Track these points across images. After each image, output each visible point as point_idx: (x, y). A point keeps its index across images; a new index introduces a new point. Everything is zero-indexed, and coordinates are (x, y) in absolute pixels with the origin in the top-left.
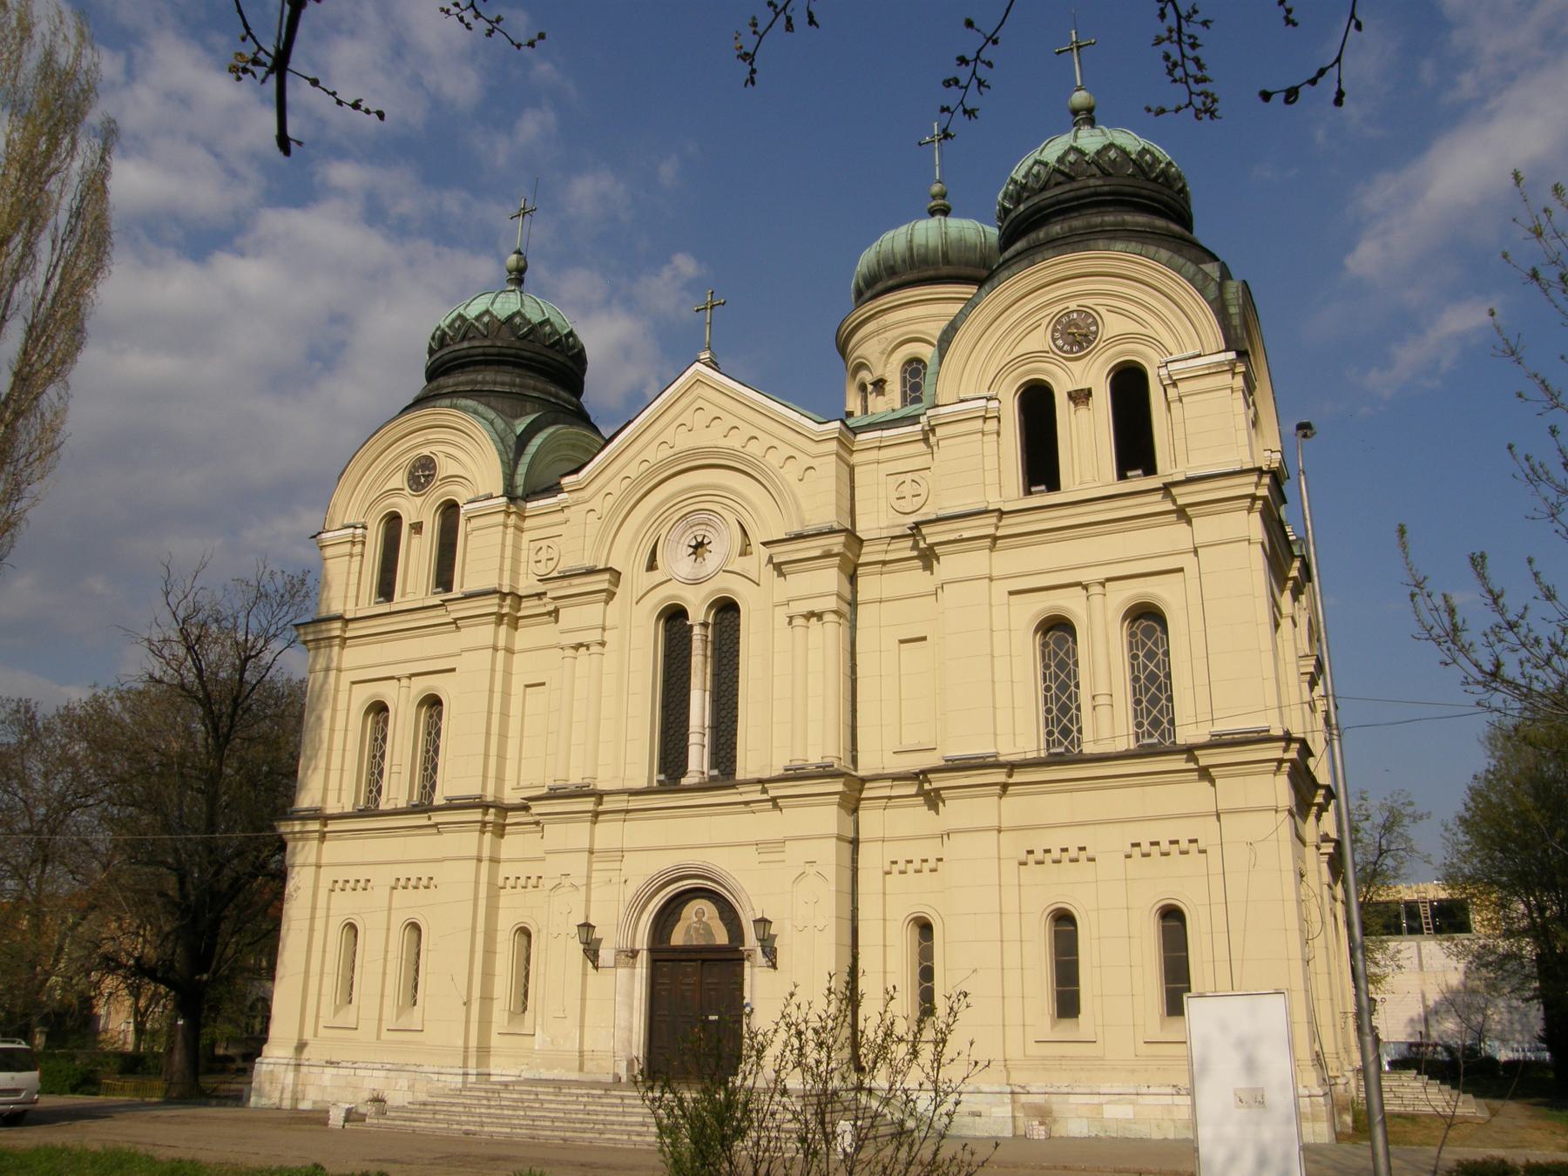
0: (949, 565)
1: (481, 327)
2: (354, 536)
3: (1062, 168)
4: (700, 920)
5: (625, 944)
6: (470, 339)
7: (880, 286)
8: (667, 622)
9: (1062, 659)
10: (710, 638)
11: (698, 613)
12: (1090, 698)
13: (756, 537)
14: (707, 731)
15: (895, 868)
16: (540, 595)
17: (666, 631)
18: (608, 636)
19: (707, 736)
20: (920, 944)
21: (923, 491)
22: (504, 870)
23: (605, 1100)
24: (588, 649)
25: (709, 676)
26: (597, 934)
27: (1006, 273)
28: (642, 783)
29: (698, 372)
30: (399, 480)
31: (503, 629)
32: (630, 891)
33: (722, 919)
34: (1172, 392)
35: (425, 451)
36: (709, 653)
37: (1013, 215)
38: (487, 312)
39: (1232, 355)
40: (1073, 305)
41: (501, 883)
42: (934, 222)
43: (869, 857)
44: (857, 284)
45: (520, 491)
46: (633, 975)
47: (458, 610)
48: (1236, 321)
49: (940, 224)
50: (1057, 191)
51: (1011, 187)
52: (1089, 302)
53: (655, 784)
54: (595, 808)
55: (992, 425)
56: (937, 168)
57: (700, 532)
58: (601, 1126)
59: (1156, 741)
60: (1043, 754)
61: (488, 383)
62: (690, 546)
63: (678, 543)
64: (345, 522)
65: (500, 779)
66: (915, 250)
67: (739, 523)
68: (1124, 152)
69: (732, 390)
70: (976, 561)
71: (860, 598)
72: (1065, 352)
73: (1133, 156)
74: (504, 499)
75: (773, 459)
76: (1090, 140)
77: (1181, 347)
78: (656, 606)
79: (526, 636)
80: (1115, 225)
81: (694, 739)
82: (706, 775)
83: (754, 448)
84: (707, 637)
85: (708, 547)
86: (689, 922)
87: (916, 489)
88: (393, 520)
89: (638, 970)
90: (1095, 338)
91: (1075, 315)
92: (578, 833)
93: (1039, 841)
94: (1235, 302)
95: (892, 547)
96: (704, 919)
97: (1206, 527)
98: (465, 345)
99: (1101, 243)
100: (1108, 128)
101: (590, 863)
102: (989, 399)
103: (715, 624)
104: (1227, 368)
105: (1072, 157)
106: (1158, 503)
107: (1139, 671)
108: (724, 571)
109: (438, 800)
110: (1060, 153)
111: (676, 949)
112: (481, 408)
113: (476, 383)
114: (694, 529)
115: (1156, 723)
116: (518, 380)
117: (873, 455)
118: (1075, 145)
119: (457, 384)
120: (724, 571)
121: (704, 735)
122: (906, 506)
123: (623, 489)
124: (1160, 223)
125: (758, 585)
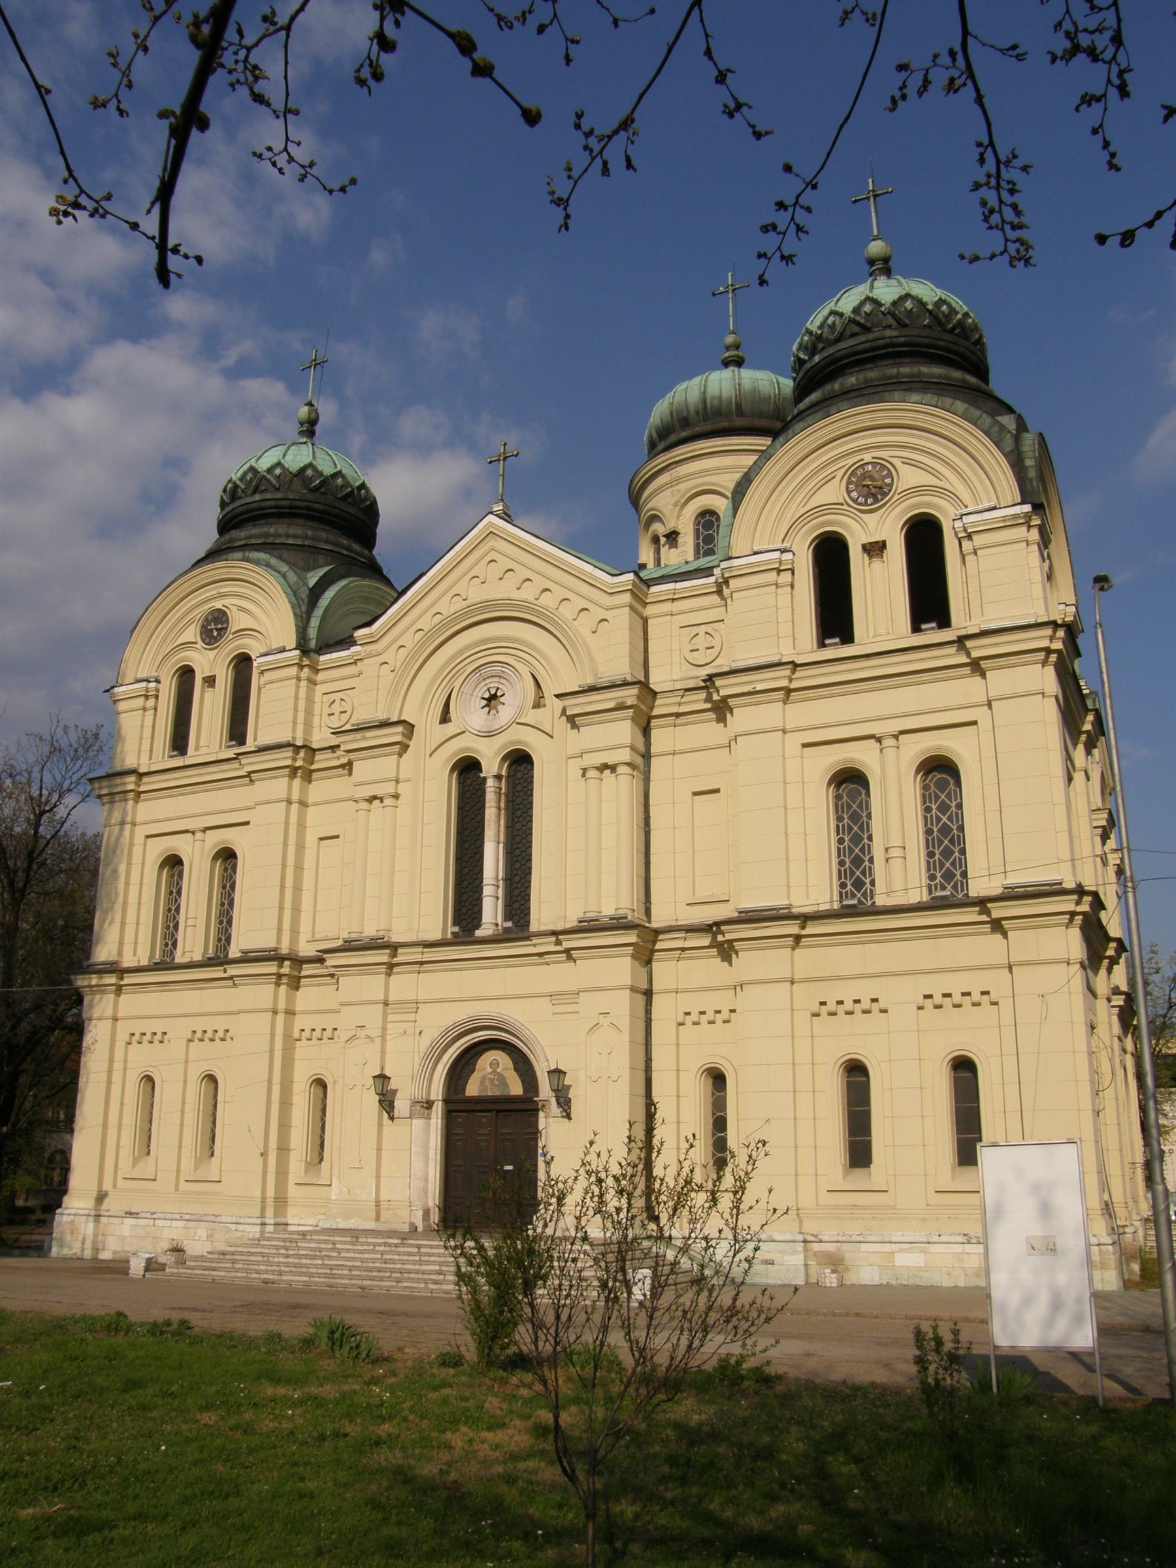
0: (742, 717)
1: (272, 480)
2: (147, 690)
3: (858, 318)
4: (494, 1072)
5: (421, 1095)
6: (262, 492)
10: (503, 791)
11: (491, 766)
13: (550, 690)
14: (501, 883)
16: (333, 748)
18: (401, 789)
20: (713, 1094)
21: (716, 643)
22: (300, 1022)
25: (502, 829)
26: (393, 1085)
27: (801, 425)
28: (436, 935)
30: (192, 633)
31: (297, 782)
32: (425, 1042)
33: (516, 1070)
34: (966, 545)
35: (218, 605)
36: (502, 805)
37: (808, 366)
38: (279, 464)
39: (1027, 508)
40: (868, 457)
41: (296, 1035)
46: (428, 1126)
47: (252, 763)
48: (1032, 474)
53: (449, 936)
55: (786, 577)
57: (493, 684)
60: (836, 906)
61: (280, 536)
62: (483, 698)
63: (472, 695)
64: (138, 676)
65: (295, 932)
68: (920, 302)
70: (771, 713)
71: (653, 750)
72: (860, 504)
73: (930, 307)
74: (297, 652)
75: (567, 612)
76: (886, 291)
77: (976, 498)
78: (447, 761)
79: (319, 790)
81: (487, 891)
82: (500, 927)
83: (547, 600)
84: (500, 789)
85: (502, 700)
86: (482, 1073)
88: (186, 674)
89: (433, 1121)
90: (890, 491)
91: (870, 467)
92: (372, 986)
94: (1031, 454)
96: (499, 1070)
97: (999, 680)
98: (257, 497)
99: (896, 395)
101: (385, 1015)
102: (783, 551)
103: (508, 776)
105: (868, 308)
107: (932, 824)
108: (518, 723)
109: (234, 952)
110: (856, 304)
112: (274, 561)
113: (269, 536)
114: (488, 681)
115: (948, 876)
117: (667, 607)
118: (871, 295)
120: (518, 723)
121: (498, 887)
124: (957, 374)
125: (552, 737)
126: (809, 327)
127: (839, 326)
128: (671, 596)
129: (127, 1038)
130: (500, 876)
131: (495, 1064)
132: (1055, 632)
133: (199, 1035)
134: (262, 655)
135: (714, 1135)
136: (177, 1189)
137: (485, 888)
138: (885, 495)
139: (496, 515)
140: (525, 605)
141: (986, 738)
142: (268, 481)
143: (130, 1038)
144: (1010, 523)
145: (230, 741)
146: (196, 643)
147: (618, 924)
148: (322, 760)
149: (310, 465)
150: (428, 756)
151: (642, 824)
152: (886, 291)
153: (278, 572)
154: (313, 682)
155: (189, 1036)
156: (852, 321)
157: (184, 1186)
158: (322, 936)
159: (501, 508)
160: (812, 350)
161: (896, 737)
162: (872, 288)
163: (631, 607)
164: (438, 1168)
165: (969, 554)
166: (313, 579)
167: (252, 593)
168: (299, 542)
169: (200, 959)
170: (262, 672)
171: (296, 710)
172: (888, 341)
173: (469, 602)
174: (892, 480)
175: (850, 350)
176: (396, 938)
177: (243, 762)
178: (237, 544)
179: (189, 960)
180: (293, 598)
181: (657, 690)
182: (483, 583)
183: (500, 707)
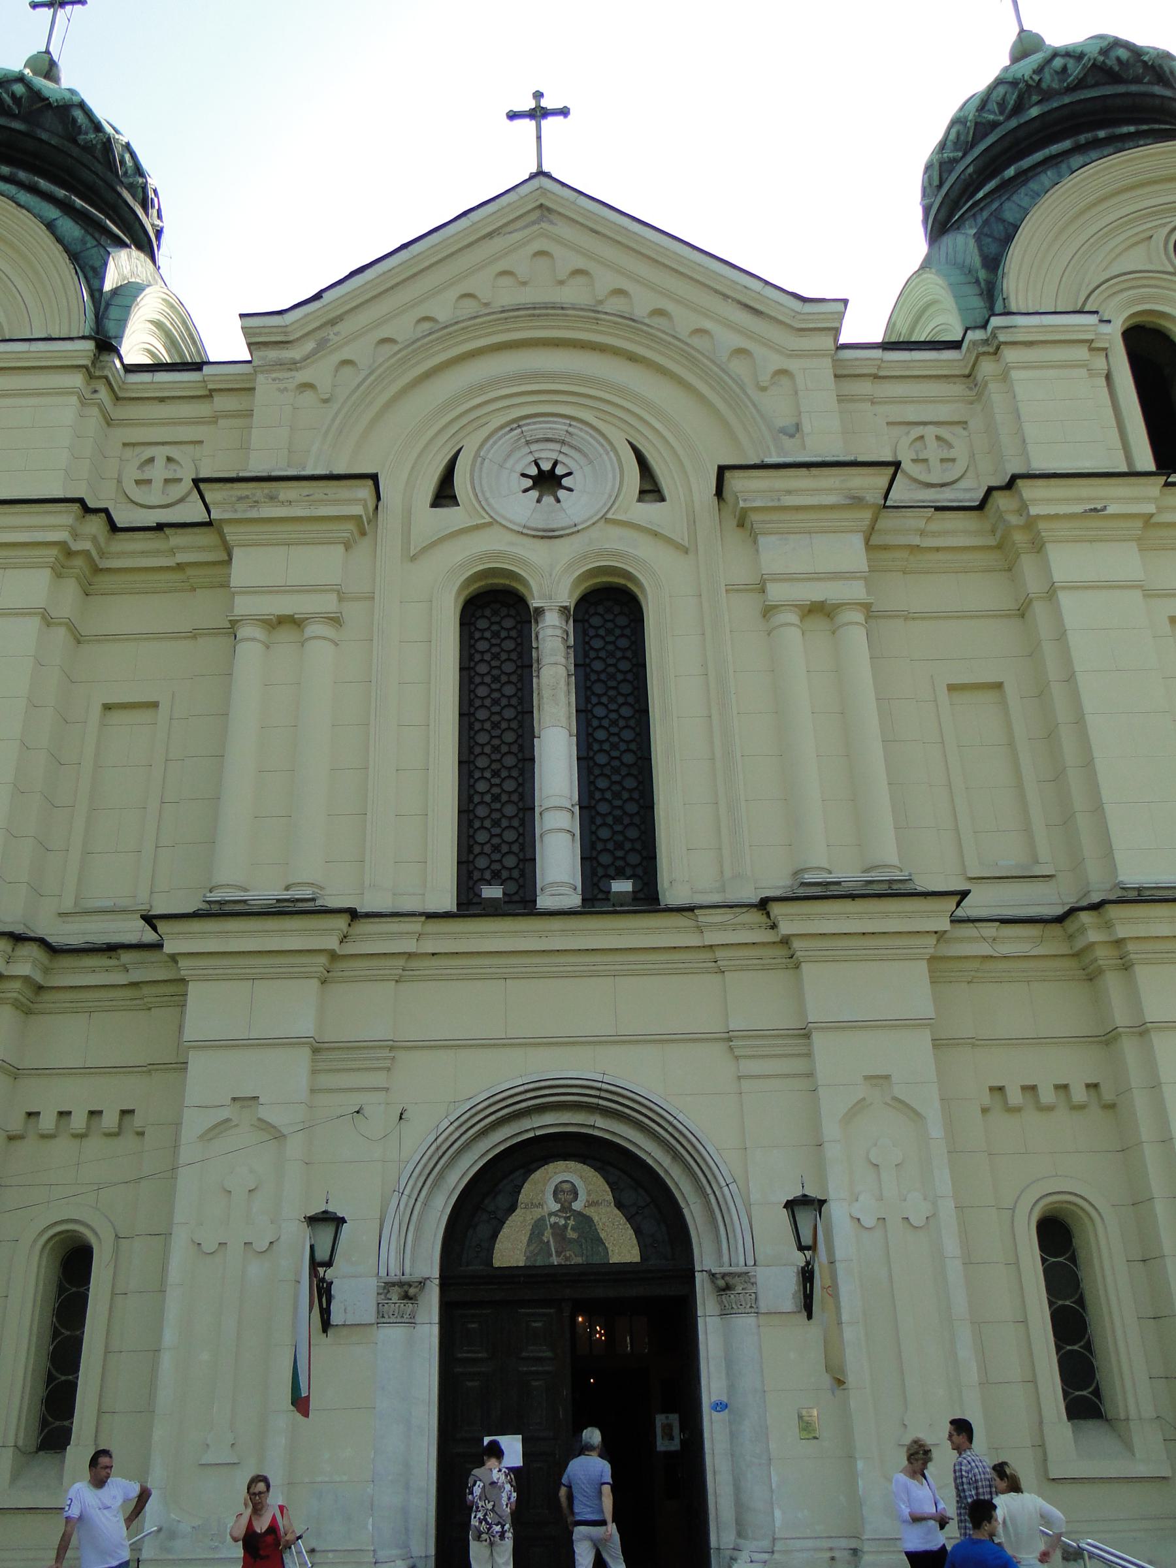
4: (566, 1208)
31: (71, 587)
33: (619, 1205)
63: (528, 443)
67: (630, 443)
80: (544, 531)
85: (565, 482)
86: (537, 1213)
95: (934, 526)
96: (577, 1206)
111: (511, 1275)
114: (534, 447)
120: (608, 521)
128: (874, 371)
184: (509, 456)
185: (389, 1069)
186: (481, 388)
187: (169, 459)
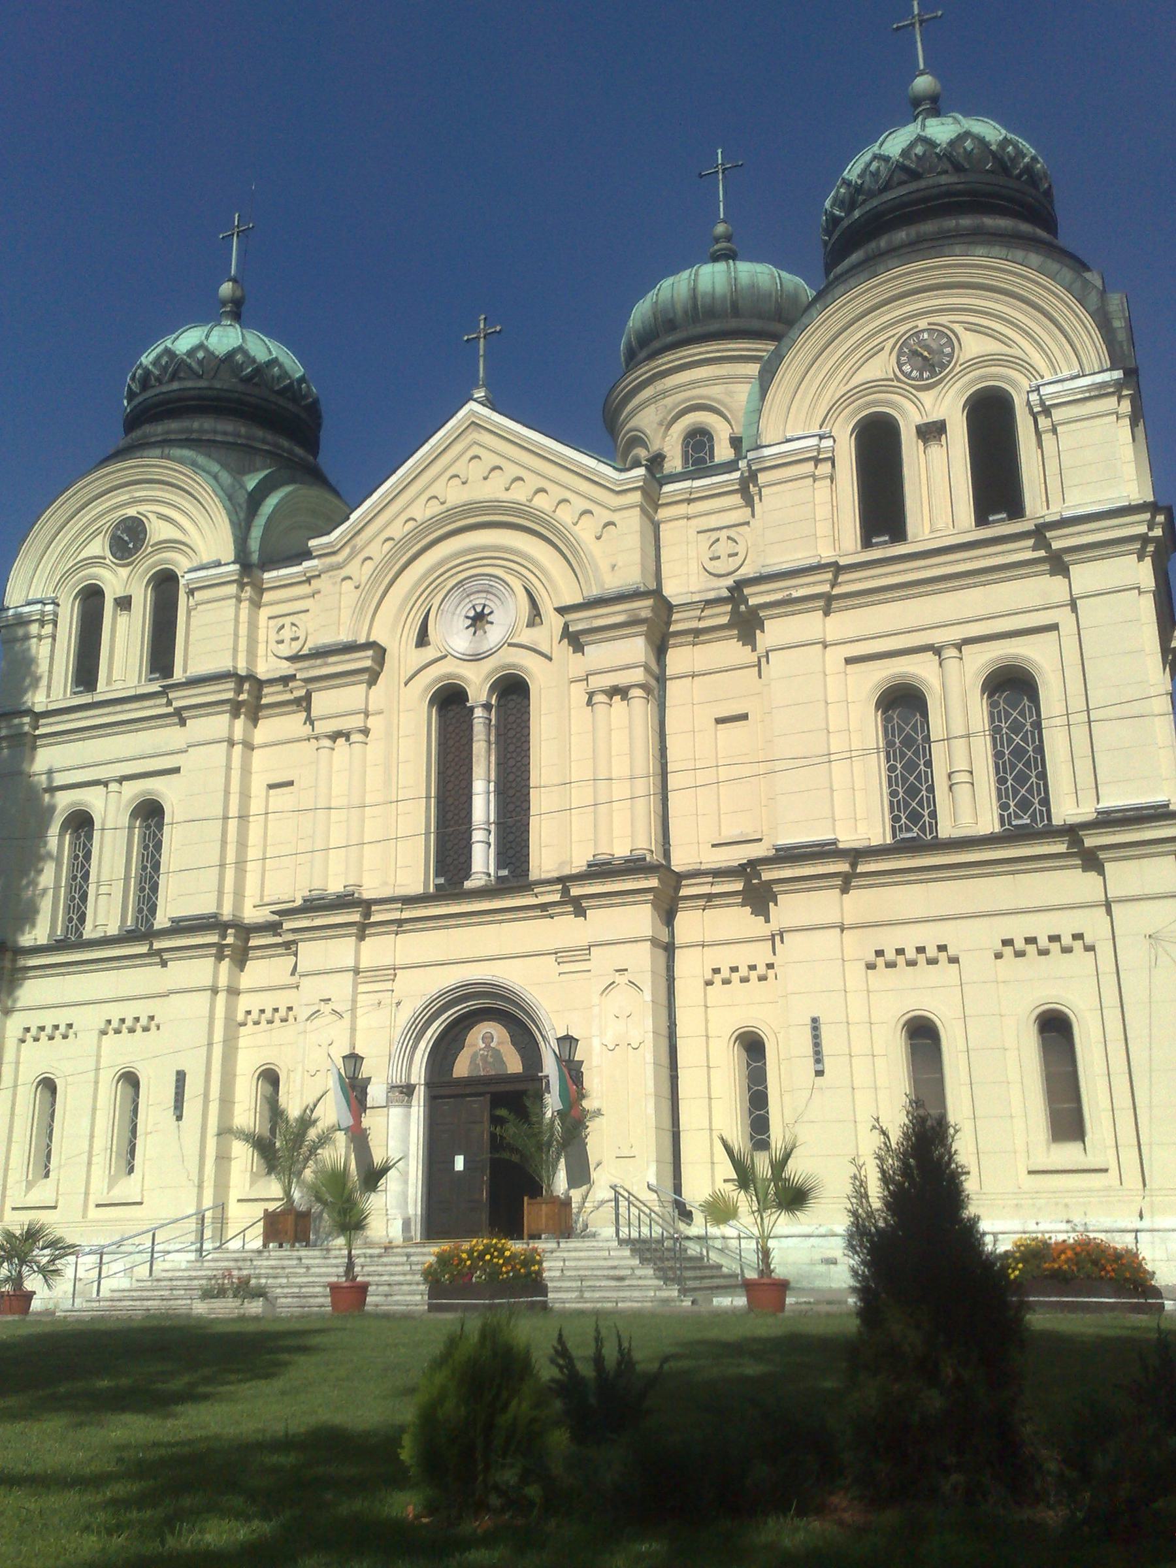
0: (775, 631)
1: (194, 365)
2: (43, 613)
3: (907, 163)
4: (488, 1046)
5: (399, 1079)
6: (180, 379)
7: (656, 345)
8: (440, 710)
9: (908, 735)
10: (493, 722)
11: (478, 691)
12: (945, 778)
13: (547, 608)
14: (493, 827)
15: (718, 979)
16: (285, 680)
17: (440, 716)
18: (372, 722)
19: (493, 833)
20: (748, 1065)
21: (741, 549)
22: (244, 1002)
23: (385, 1260)
24: (348, 739)
25: (493, 766)
26: (365, 1072)
27: (841, 288)
28: (417, 889)
29: (473, 413)
30: (98, 546)
32: (405, 1015)
33: (514, 1043)
34: (1044, 422)
35: (131, 512)
36: (493, 739)
37: (845, 223)
38: (201, 346)
39: (1118, 374)
40: (922, 324)
41: (240, 1017)
42: (721, 267)
43: (689, 966)
44: (629, 343)
45: (255, 557)
46: (408, 1116)
47: (181, 699)
48: (1122, 336)
49: (729, 268)
50: (902, 190)
51: (842, 190)
52: (943, 319)
53: (432, 889)
54: (362, 920)
55: (825, 468)
56: (721, 204)
57: (479, 600)
58: (386, 1288)
59: (915, 835)
60: (889, 840)
61: (206, 432)
62: (467, 617)
63: (454, 614)
64: (30, 598)
65: (239, 894)
66: (699, 299)
68: (981, 141)
69: (510, 432)
70: (809, 624)
71: (669, 672)
72: (913, 379)
73: (994, 147)
74: (236, 567)
75: (565, 515)
76: (941, 130)
77: (1054, 369)
78: (426, 690)
79: (268, 729)
81: (478, 835)
82: (492, 878)
83: (541, 502)
84: (490, 720)
85: (490, 618)
87: (731, 547)
88: (92, 597)
89: (414, 1110)
90: (950, 362)
91: (926, 336)
92: (341, 950)
93: (889, 940)
94: (1121, 315)
96: (492, 1045)
97: (1085, 576)
98: (175, 385)
99: (957, 249)
100: (964, 116)
101: (355, 985)
102: (821, 437)
103: (499, 706)
104: (1111, 390)
105: (919, 150)
106: (1025, 551)
107: (1002, 745)
108: (510, 645)
109: (161, 921)
110: (904, 145)
112: (201, 460)
113: (192, 431)
114: (472, 597)
115: (1024, 805)
116: (243, 430)
117: (682, 509)
118: (923, 134)
119: (168, 433)
120: (510, 645)
121: (490, 832)
122: (719, 567)
123: (384, 552)
124: (1025, 227)
125: (550, 659)
126: (847, 177)
127: (884, 173)
129: (20, 1034)
130: (492, 819)
131: (488, 1038)
132: (1153, 517)
133: (115, 1024)
134: (190, 571)
135: (751, 1113)
136: (84, 1216)
137: (474, 833)
138: (943, 366)
139: (479, 402)
140: (516, 509)
141: (1070, 644)
142: (189, 367)
143: (24, 1035)
144: (1099, 392)
145: (151, 673)
146: (104, 558)
147: (634, 866)
148: (271, 695)
149: (240, 349)
150: (402, 685)
151: (658, 754)
152: (941, 130)
153: (208, 472)
154: (256, 604)
155: (102, 1026)
156: (901, 167)
157: (93, 1213)
158: (274, 898)
159: (483, 394)
160: (849, 204)
161: (958, 646)
162: (923, 127)
163: (643, 511)
164: (420, 1167)
165: (1046, 431)
166: (251, 482)
167: (179, 500)
168: (231, 439)
169: (116, 933)
170: (191, 592)
171: (236, 635)
172: (944, 189)
173: (448, 505)
174: (953, 349)
175: (897, 201)
176: (367, 895)
177: (171, 696)
178: (153, 440)
179: (103, 935)
180: (228, 503)
181: (674, 603)
182: (464, 483)
183: (488, 627)
184: (456, 609)
185: (394, 980)
186: (441, 563)
187: (293, 624)
